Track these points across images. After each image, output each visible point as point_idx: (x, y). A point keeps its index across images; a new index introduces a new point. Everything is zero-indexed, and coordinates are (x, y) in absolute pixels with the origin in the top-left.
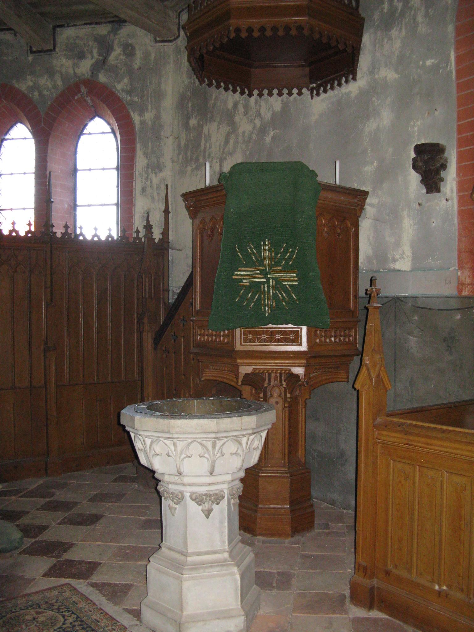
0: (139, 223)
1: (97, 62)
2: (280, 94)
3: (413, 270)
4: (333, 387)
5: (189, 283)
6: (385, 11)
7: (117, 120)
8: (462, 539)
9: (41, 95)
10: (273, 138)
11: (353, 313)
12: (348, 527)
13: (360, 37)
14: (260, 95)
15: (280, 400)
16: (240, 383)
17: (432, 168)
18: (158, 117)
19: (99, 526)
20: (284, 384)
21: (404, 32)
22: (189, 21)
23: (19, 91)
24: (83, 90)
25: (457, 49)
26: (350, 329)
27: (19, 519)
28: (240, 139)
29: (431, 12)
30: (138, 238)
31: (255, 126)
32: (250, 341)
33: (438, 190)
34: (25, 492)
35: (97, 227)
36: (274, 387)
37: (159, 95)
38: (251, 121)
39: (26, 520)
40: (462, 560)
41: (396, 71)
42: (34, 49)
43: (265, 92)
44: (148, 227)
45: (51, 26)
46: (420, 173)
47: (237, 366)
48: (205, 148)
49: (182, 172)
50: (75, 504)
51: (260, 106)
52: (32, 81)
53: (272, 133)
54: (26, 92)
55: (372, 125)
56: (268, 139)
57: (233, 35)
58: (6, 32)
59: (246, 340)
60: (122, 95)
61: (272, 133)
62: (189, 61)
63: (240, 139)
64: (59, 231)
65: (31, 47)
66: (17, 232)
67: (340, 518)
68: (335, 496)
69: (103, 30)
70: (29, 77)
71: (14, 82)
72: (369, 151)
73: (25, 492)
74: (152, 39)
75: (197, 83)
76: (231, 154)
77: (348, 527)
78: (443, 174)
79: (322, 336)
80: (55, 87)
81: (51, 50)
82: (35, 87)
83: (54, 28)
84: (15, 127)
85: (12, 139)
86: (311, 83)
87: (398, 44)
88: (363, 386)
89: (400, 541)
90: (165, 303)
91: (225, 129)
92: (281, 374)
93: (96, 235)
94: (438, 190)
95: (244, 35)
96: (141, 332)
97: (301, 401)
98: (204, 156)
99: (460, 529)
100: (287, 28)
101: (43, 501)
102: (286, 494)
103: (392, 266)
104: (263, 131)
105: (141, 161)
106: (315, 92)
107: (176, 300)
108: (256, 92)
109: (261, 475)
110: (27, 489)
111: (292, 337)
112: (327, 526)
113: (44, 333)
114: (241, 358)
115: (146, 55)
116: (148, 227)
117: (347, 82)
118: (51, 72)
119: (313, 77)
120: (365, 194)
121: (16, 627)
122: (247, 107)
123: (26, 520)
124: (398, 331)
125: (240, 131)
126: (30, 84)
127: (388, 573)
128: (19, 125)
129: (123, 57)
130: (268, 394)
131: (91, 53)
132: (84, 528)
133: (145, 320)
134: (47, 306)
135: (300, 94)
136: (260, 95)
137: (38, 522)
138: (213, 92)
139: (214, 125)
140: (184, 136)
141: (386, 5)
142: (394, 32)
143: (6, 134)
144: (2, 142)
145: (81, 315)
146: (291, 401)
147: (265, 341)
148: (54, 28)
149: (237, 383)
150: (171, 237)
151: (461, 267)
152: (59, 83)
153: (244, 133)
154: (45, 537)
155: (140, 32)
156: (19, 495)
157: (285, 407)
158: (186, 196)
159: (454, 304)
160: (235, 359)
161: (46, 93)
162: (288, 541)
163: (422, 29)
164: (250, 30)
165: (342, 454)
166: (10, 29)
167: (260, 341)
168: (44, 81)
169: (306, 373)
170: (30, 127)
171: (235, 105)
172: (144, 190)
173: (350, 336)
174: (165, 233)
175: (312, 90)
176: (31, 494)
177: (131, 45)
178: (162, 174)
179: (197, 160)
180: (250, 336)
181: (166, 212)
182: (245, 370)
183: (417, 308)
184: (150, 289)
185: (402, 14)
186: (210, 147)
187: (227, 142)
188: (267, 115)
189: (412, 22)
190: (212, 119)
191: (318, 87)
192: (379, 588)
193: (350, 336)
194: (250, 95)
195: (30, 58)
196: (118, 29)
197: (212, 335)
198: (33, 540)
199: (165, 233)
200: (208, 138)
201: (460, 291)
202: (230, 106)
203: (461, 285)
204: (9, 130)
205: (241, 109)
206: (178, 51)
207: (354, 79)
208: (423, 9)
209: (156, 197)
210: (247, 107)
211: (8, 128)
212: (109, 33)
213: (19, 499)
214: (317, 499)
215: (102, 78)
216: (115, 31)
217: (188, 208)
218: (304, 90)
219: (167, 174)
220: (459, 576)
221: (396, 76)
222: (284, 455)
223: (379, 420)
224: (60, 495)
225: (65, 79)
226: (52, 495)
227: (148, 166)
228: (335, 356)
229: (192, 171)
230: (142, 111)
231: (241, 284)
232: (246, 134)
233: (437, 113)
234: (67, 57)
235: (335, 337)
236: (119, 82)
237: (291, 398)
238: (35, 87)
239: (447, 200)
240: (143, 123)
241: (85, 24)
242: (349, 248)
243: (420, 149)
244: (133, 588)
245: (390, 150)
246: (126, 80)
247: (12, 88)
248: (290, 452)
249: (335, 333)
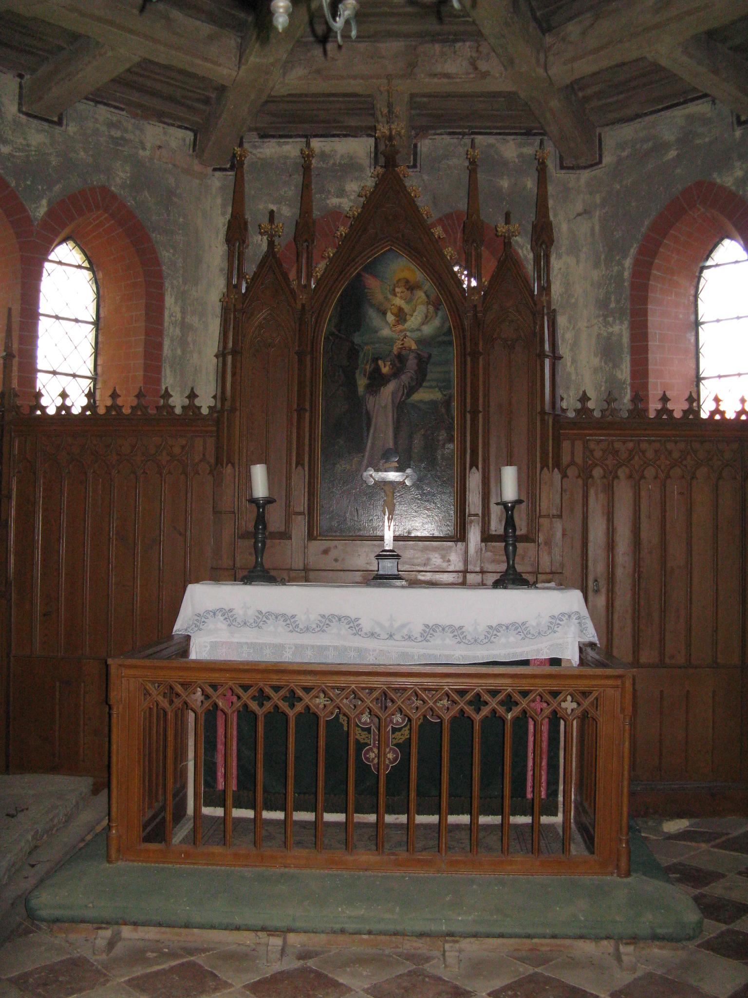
23: (722, 188)
27: (707, 884)
34: (723, 839)
35: (746, 398)
52: (741, 169)
54: (733, 188)
58: (700, 101)
65: (738, 117)
66: (722, 413)
70: (738, 164)
71: (715, 175)
73: (723, 839)
84: (720, 245)
85: (717, 265)
110: (727, 834)
121: (108, 981)
123: (716, 890)
128: (727, 242)
143: (707, 259)
144: (701, 272)
156: (713, 843)
166: (705, 95)
170: (742, 242)
198: (724, 927)
204: (711, 251)
211: (710, 248)
213: (712, 849)
244: (353, 993)
247: (713, 184)
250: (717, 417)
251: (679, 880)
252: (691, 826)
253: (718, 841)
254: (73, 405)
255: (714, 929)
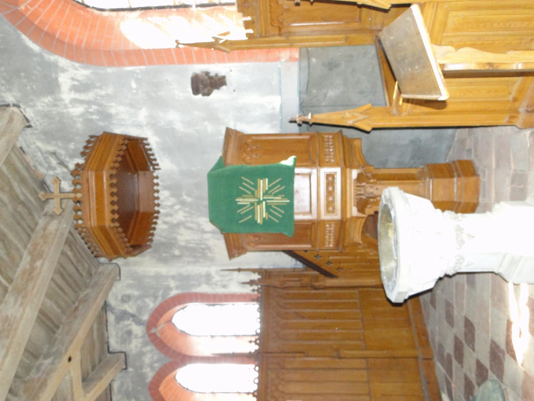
0: (248, 290)
1: (134, 321)
2: (158, 191)
3: (280, 94)
4: (364, 149)
5: (291, 253)
6: (98, 117)
7: (175, 306)
8: (491, 42)
9: (156, 362)
10: (188, 195)
11: (312, 137)
12: (470, 135)
13: (115, 136)
14: (158, 205)
15: (375, 186)
16: (364, 216)
17: (208, 82)
18: (173, 277)
19: (475, 320)
20: (363, 184)
21: (113, 104)
22: (107, 255)
23: (154, 378)
24: (153, 331)
25: (123, 65)
26: (323, 138)
27: (471, 382)
28: (189, 219)
29: (98, 84)
30: (258, 290)
31: (179, 209)
32: (334, 208)
33: (224, 77)
36: (365, 191)
37: (158, 277)
38: (176, 211)
39: (473, 377)
40: (507, 42)
41: (140, 109)
42: (124, 367)
43: (156, 202)
44: (252, 283)
45: (108, 355)
46: (213, 91)
47: (352, 218)
48: (196, 244)
49: (212, 260)
50: (456, 338)
51: (166, 206)
53: (185, 197)
55: (179, 127)
56: (189, 200)
57: (117, 224)
59: (333, 211)
60: (158, 302)
61: (185, 197)
62: (134, 256)
63: (189, 219)
64: (253, 348)
65: (123, 369)
67: (462, 142)
68: (444, 146)
69: (111, 318)
70: (144, 370)
72: (197, 128)
74: (118, 282)
75: (149, 250)
76: (199, 225)
77: (470, 135)
78: (212, 74)
79: (330, 158)
80: (151, 351)
81: (126, 355)
82: (151, 366)
83: (109, 352)
86: (149, 170)
87: (121, 108)
88: (369, 125)
89: (490, 92)
90: (303, 271)
91: (182, 230)
92: (357, 186)
93: (255, 342)
94: (224, 77)
95: (116, 216)
96: (326, 288)
97: (375, 172)
98: (201, 244)
99: (483, 44)
100: (112, 185)
101: (455, 363)
102: (446, 181)
103: (278, 110)
104: (183, 203)
105: (204, 289)
106: (155, 166)
107: (300, 261)
108: (156, 208)
109: (281, 216)
110: (445, 375)
111: (330, 179)
112: (469, 151)
113: (327, 359)
114: (346, 214)
115: (129, 286)
116: (252, 283)
117: (148, 144)
118: (141, 354)
119: (146, 169)
120: (228, 130)
122: (167, 215)
123: (473, 377)
124: (324, 104)
125: (183, 219)
126: (148, 370)
127: (515, 100)
129: (131, 303)
130: (371, 195)
131: (128, 325)
132: (477, 333)
133: (317, 284)
134: (308, 356)
135: (157, 178)
136: (158, 205)
137: (474, 367)
138: (156, 238)
139: (180, 238)
140: (186, 259)
141: (94, 117)
142: (113, 111)
145: (313, 331)
146: (253, 222)
147: (334, 198)
148: (109, 352)
149: (363, 217)
150: (257, 267)
151: (278, 59)
152: (148, 348)
153: (185, 217)
154: (487, 363)
155: (114, 289)
157: (380, 183)
158: (231, 256)
159: (305, 63)
160: (347, 219)
161: (155, 358)
162: (481, 178)
163: (110, 90)
164: (113, 212)
165: (413, 142)
167: (333, 201)
168: (147, 359)
169: (357, 168)
171: (165, 223)
172: (224, 286)
173: (328, 138)
174: (254, 271)
175: (155, 169)
176: (449, 371)
177: (122, 297)
178: (213, 274)
179: (203, 249)
180: (331, 209)
181: (239, 270)
182: (354, 211)
183: (308, 91)
184: (295, 281)
185: (100, 105)
186: (195, 240)
187: (190, 228)
188: (172, 201)
189: (105, 98)
190: (175, 239)
191: (154, 165)
192: (527, 107)
193: (328, 138)
194: (158, 212)
195: (130, 369)
196: (111, 307)
197: (330, 236)
198: (490, 372)
199: (254, 271)
200: (188, 241)
201: (295, 60)
202: (165, 227)
203: (291, 59)
205: (168, 219)
206: (126, 264)
207: (146, 139)
208: (96, 90)
209: (229, 277)
210: (167, 215)
212: (113, 313)
214: (445, 160)
215: (145, 317)
216: (112, 310)
217: (240, 254)
218: (155, 174)
219: (213, 270)
220: (520, 43)
221: (144, 109)
222: (417, 183)
223: (394, 111)
224: (449, 349)
225: (145, 344)
226: (449, 355)
227: (207, 283)
228: (344, 148)
229: (211, 252)
230: (169, 289)
231: (267, 218)
232: (185, 215)
233: (170, 80)
234: (130, 343)
235: (329, 148)
236: (148, 306)
237: (373, 179)
238: (151, 366)
239: (231, 71)
240: (177, 288)
241: (107, 330)
242: (266, 141)
243: (196, 91)
245: (196, 113)
246: (147, 300)
247: (151, 383)
248: (413, 179)
249: (327, 148)
250: (258, 342)
251: (472, 395)
252: (444, 393)
253: (449, 378)
254: (258, 318)
255: (491, 375)
